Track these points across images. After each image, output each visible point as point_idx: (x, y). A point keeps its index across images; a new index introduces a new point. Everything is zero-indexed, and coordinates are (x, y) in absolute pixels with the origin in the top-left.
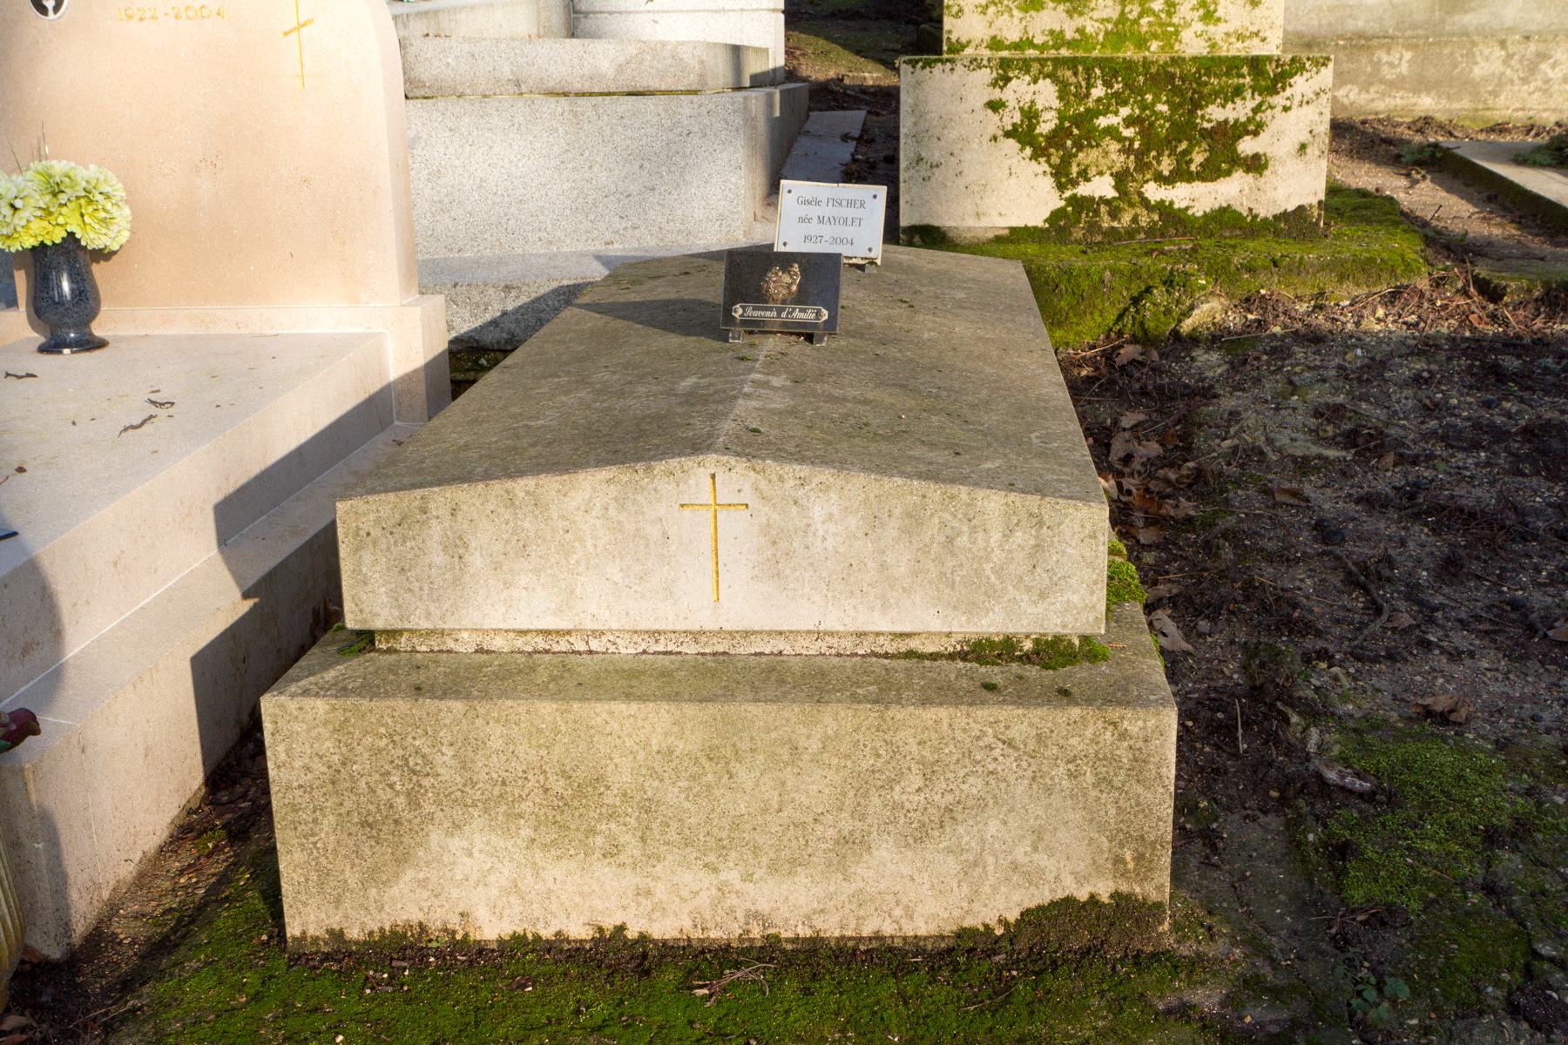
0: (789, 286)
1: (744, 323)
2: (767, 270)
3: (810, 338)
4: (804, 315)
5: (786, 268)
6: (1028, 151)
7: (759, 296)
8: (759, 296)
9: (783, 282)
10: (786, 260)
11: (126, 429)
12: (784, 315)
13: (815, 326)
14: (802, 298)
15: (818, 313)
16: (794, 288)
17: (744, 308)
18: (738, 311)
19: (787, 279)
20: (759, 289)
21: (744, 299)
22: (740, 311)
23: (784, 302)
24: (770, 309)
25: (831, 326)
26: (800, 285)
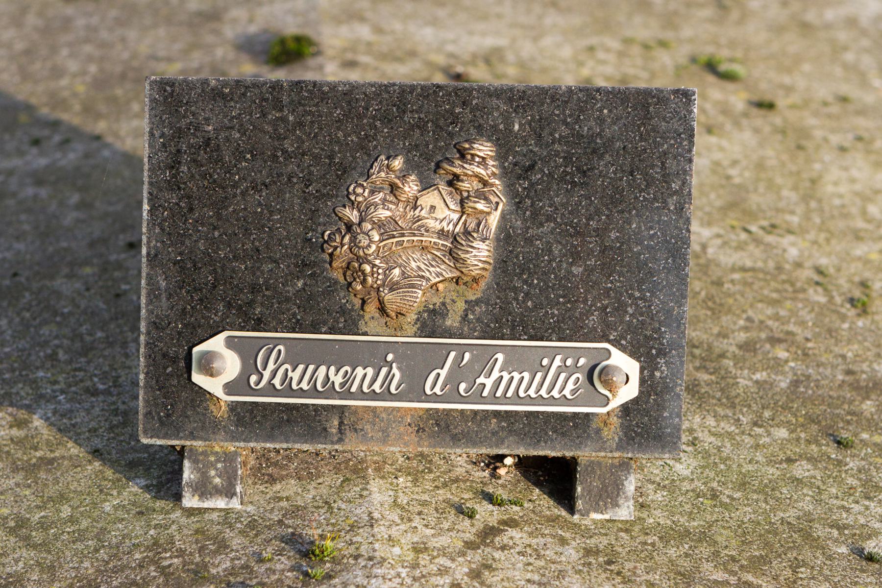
0: (455, 245)
1: (252, 419)
2: (339, 174)
3: (556, 478)
4: (536, 379)
5: (434, 162)
6: (736, 267)
7: (312, 296)
8: (312, 296)
9: (428, 228)
10: (430, 121)
11: (627, 376)
12: (436, 381)
13: (579, 425)
14: (522, 301)
15: (597, 375)
16: (480, 254)
17: (248, 354)
18: (221, 365)
19: (439, 210)
20: (310, 258)
21: (248, 312)
22: (231, 365)
23: (431, 322)
24: (375, 356)
25: (646, 425)
26: (506, 239)
